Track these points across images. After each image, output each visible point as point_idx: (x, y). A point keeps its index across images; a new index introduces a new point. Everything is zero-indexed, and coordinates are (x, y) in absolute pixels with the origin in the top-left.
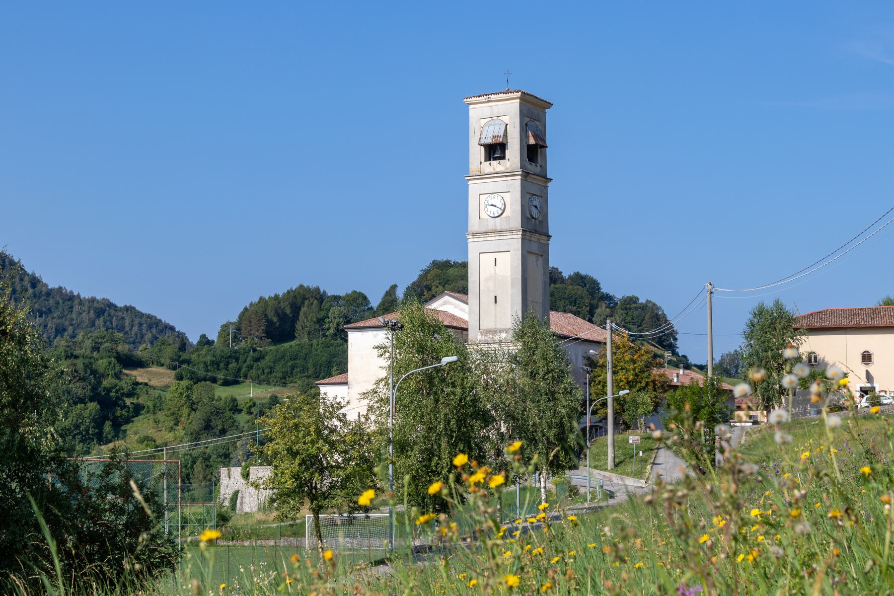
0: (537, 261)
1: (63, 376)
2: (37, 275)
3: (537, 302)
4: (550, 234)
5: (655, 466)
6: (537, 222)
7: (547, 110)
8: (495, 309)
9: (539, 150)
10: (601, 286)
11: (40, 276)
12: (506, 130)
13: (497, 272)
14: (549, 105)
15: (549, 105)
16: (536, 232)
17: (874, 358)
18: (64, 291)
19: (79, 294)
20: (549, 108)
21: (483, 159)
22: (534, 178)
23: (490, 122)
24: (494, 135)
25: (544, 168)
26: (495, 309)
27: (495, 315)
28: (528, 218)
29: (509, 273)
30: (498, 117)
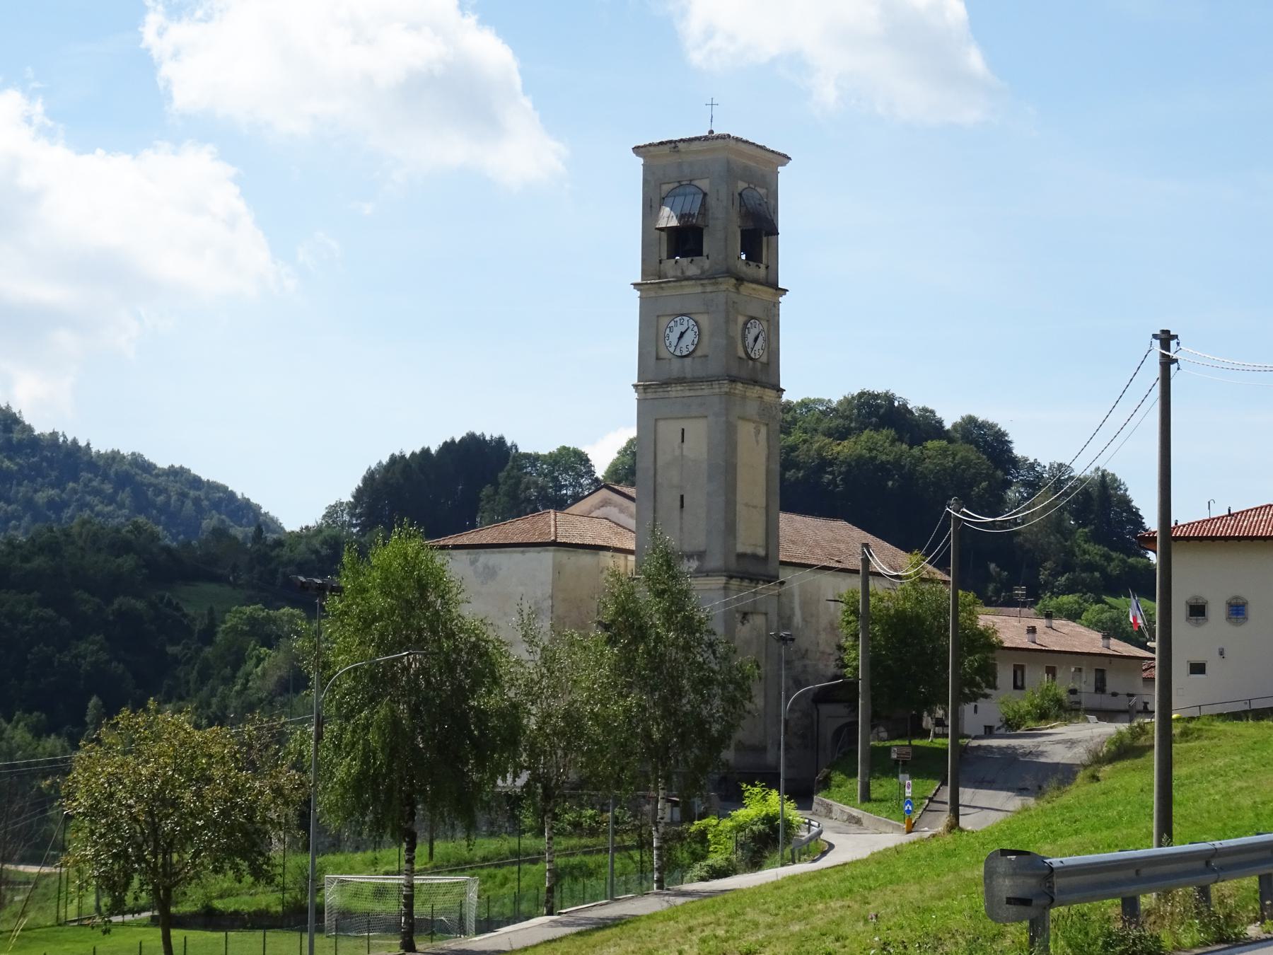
0: (758, 432)
1: (724, 419)
2: (15, 410)
3: (755, 507)
4: (782, 386)
5: (777, 598)
6: (758, 365)
7: (780, 169)
8: (681, 518)
9: (765, 239)
10: (632, 437)
11: (20, 412)
12: (704, 204)
13: (684, 453)
14: (785, 158)
15: (785, 158)
16: (755, 382)
17: (1252, 611)
18: (61, 439)
19: (88, 444)
20: (784, 164)
21: (664, 255)
22: (754, 289)
23: (677, 190)
24: (683, 212)
25: (773, 269)
26: (681, 518)
27: (681, 529)
28: (740, 358)
29: (705, 456)
30: (691, 181)
